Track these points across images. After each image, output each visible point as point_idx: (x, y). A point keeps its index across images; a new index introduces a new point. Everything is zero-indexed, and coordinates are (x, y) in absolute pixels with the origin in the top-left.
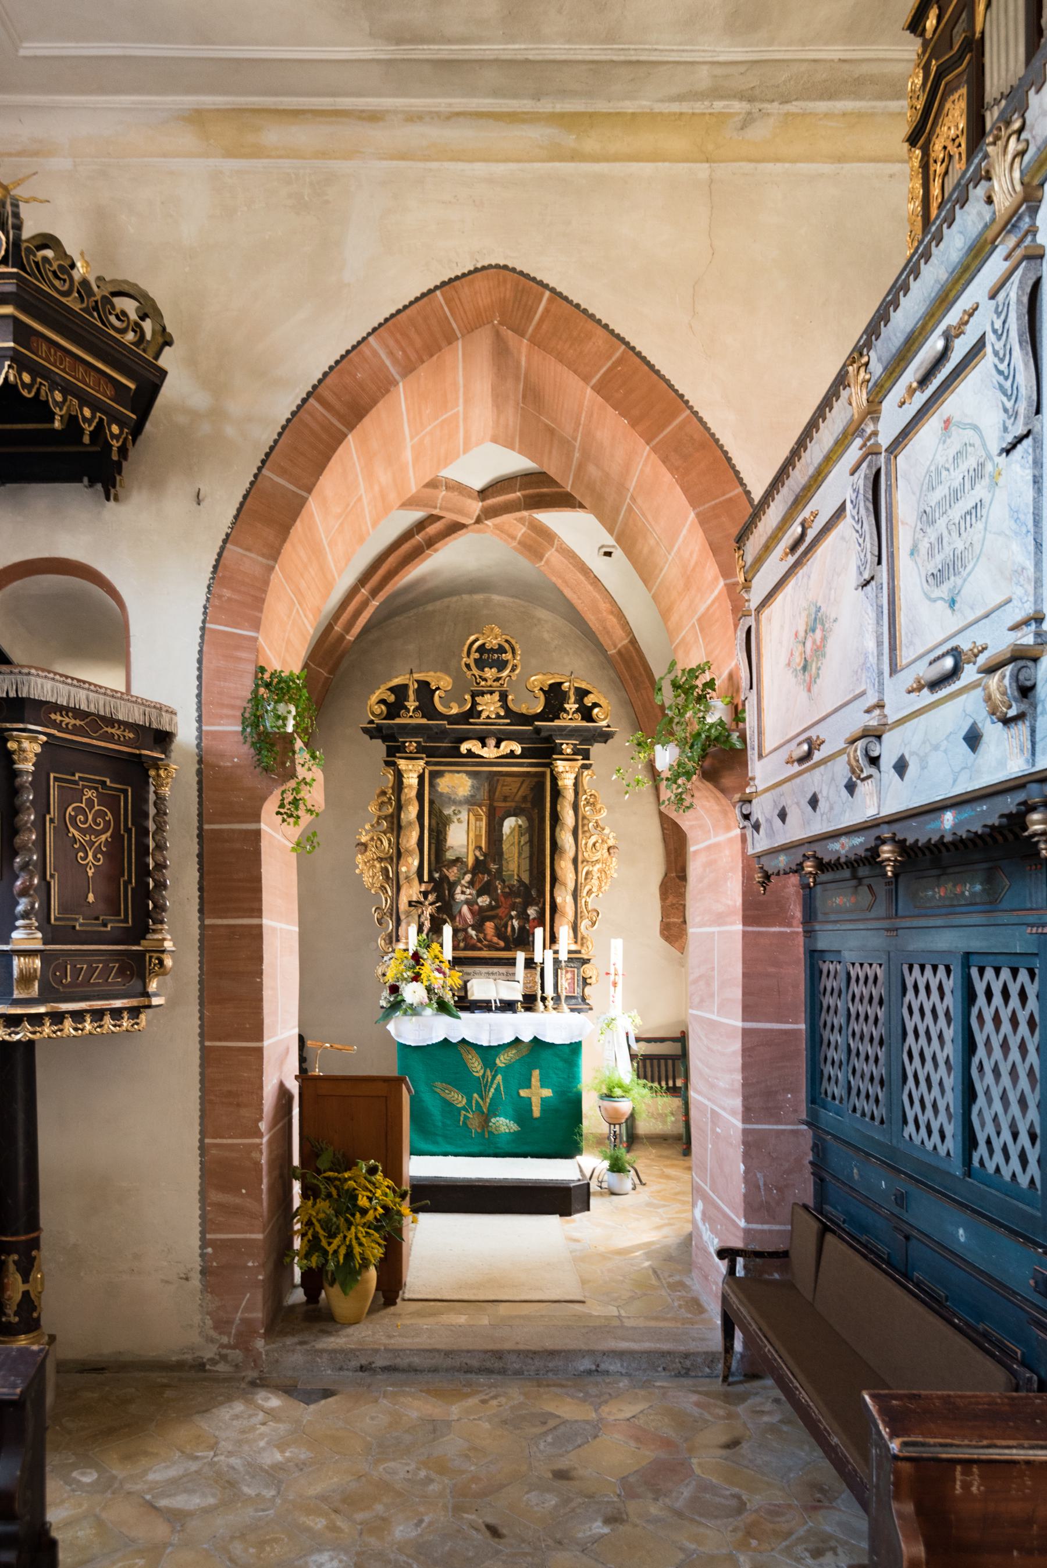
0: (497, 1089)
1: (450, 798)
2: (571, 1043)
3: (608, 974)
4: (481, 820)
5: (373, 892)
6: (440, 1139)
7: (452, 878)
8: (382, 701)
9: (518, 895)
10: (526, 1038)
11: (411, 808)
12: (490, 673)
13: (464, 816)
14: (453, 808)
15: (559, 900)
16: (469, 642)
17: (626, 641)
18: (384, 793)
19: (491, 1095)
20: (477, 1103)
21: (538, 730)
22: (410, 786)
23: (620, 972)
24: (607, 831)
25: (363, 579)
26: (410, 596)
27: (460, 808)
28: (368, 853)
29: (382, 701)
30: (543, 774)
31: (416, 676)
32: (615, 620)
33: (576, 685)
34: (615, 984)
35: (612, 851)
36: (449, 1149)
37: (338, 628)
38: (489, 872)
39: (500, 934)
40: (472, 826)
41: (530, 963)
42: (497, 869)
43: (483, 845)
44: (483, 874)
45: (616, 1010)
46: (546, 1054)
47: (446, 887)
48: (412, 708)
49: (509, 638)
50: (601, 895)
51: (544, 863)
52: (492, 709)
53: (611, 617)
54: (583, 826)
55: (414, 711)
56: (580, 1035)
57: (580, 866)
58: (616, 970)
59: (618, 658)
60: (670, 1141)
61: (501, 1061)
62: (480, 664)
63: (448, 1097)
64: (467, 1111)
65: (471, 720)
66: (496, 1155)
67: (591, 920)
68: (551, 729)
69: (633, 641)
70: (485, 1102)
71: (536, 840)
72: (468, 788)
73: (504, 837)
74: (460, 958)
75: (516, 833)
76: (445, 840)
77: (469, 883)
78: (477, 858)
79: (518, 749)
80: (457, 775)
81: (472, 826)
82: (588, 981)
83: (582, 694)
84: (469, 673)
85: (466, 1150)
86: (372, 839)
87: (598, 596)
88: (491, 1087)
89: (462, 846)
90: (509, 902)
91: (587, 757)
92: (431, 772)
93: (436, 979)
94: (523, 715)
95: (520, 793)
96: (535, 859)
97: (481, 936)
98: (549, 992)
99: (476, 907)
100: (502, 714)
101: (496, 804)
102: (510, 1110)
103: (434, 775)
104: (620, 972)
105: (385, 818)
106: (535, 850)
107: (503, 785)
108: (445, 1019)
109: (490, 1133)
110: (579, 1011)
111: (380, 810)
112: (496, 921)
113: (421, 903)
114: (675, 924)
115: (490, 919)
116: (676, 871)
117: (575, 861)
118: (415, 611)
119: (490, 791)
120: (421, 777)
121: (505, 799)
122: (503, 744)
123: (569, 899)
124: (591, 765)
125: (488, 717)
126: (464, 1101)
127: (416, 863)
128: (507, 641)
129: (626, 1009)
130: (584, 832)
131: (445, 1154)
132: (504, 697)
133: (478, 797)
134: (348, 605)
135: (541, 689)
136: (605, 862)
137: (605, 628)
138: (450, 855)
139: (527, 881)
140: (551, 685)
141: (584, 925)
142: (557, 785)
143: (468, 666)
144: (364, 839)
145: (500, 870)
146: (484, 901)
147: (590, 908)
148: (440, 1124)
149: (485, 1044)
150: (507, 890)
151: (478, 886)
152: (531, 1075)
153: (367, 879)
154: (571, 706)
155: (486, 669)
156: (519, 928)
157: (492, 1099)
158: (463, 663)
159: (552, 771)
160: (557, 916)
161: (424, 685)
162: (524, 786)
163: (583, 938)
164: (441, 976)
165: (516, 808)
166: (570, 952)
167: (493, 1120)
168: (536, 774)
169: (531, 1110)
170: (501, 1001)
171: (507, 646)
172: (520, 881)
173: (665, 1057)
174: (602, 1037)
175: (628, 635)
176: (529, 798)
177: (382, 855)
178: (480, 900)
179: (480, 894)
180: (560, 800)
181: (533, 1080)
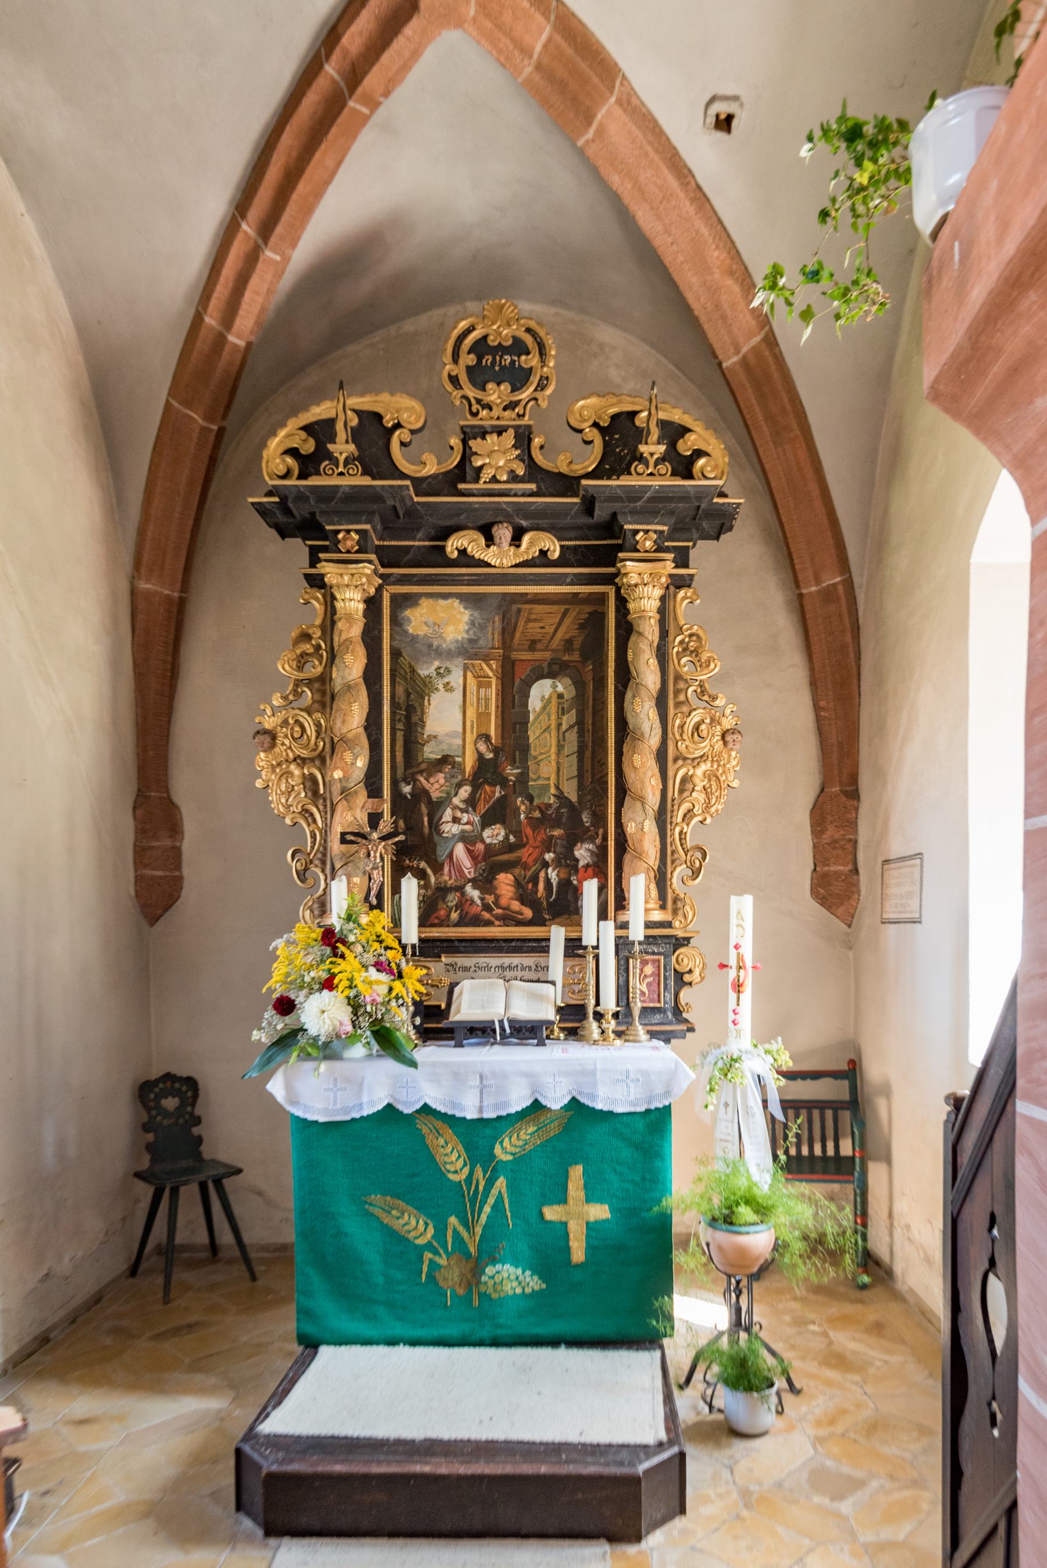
0: (498, 1206)
1: (430, 646)
2: (648, 1111)
3: (723, 966)
4: (489, 685)
5: (288, 821)
6: (381, 1311)
7: (435, 795)
8: (293, 452)
9: (556, 823)
10: (556, 1100)
11: (349, 658)
12: (496, 394)
13: (456, 678)
14: (437, 664)
15: (631, 828)
16: (455, 333)
17: (757, 339)
18: (306, 637)
20: (456, 1233)
21: (589, 504)
22: (349, 618)
23: (749, 961)
24: (720, 702)
25: (241, 207)
26: (363, 288)
27: (448, 664)
29: (293, 452)
30: (602, 598)
31: (353, 402)
33: (662, 415)
34: (738, 987)
35: (729, 738)
36: (399, 1329)
37: (210, 320)
38: (503, 782)
39: (525, 896)
40: (472, 698)
41: (574, 947)
42: (517, 776)
43: (493, 733)
44: (493, 785)
46: (597, 1133)
47: (424, 810)
50: (709, 821)
51: (604, 764)
52: (501, 463)
53: (729, 282)
54: (677, 692)
56: (667, 1093)
57: (671, 769)
58: (740, 958)
61: (505, 1150)
62: (478, 376)
64: (436, 1253)
65: (461, 486)
66: (496, 1343)
67: (691, 867)
69: (771, 341)
72: (463, 627)
74: (654, 937)
75: (553, 708)
77: (465, 801)
78: (480, 756)
79: (554, 548)
81: (472, 698)
82: (687, 978)
83: (674, 432)
84: (457, 394)
86: (285, 722)
88: (484, 1202)
89: (452, 735)
90: (542, 836)
91: (682, 559)
94: (561, 475)
95: (559, 635)
96: (588, 754)
97: (490, 899)
98: (609, 1003)
99: (480, 847)
101: (515, 655)
102: (523, 1248)
103: (401, 602)
104: (749, 961)
105: (309, 683)
106: (589, 738)
107: (529, 620)
108: (390, 1066)
109: (484, 1296)
110: (666, 1037)
111: (300, 668)
112: (517, 871)
113: (363, 836)
114: (837, 874)
115: (506, 867)
116: (841, 785)
117: (661, 756)
118: (381, 334)
119: (504, 631)
120: (372, 604)
121: (533, 645)
122: (526, 539)
123: (650, 826)
124: (691, 576)
125: (494, 479)
126: (431, 1231)
127: (362, 763)
128: (528, 330)
129: (762, 1036)
130: (678, 705)
131: (392, 1342)
133: (482, 643)
135: (595, 425)
136: (716, 759)
137: (718, 307)
138: (430, 752)
139: (574, 798)
140: (615, 417)
141: (678, 874)
142: (627, 612)
144: (269, 722)
145: (523, 778)
146: (495, 834)
147: (689, 844)
148: (380, 1280)
149: (471, 1115)
150: (537, 814)
151: (482, 808)
153: (276, 801)
155: (490, 386)
156: (560, 884)
157: (486, 1227)
158: (445, 374)
159: (618, 589)
160: (627, 858)
161: (371, 419)
162: (568, 621)
164: (383, 977)
165: (552, 663)
166: (648, 925)
167: (489, 1270)
168: (590, 599)
169: (568, 1249)
170: (511, 1022)
171: (529, 340)
172: (560, 796)
173: (821, 1105)
174: (713, 1099)
175: (762, 327)
176: (577, 644)
177: (304, 753)
178: (487, 833)
179: (487, 821)
180: (633, 638)
181: (570, 1186)
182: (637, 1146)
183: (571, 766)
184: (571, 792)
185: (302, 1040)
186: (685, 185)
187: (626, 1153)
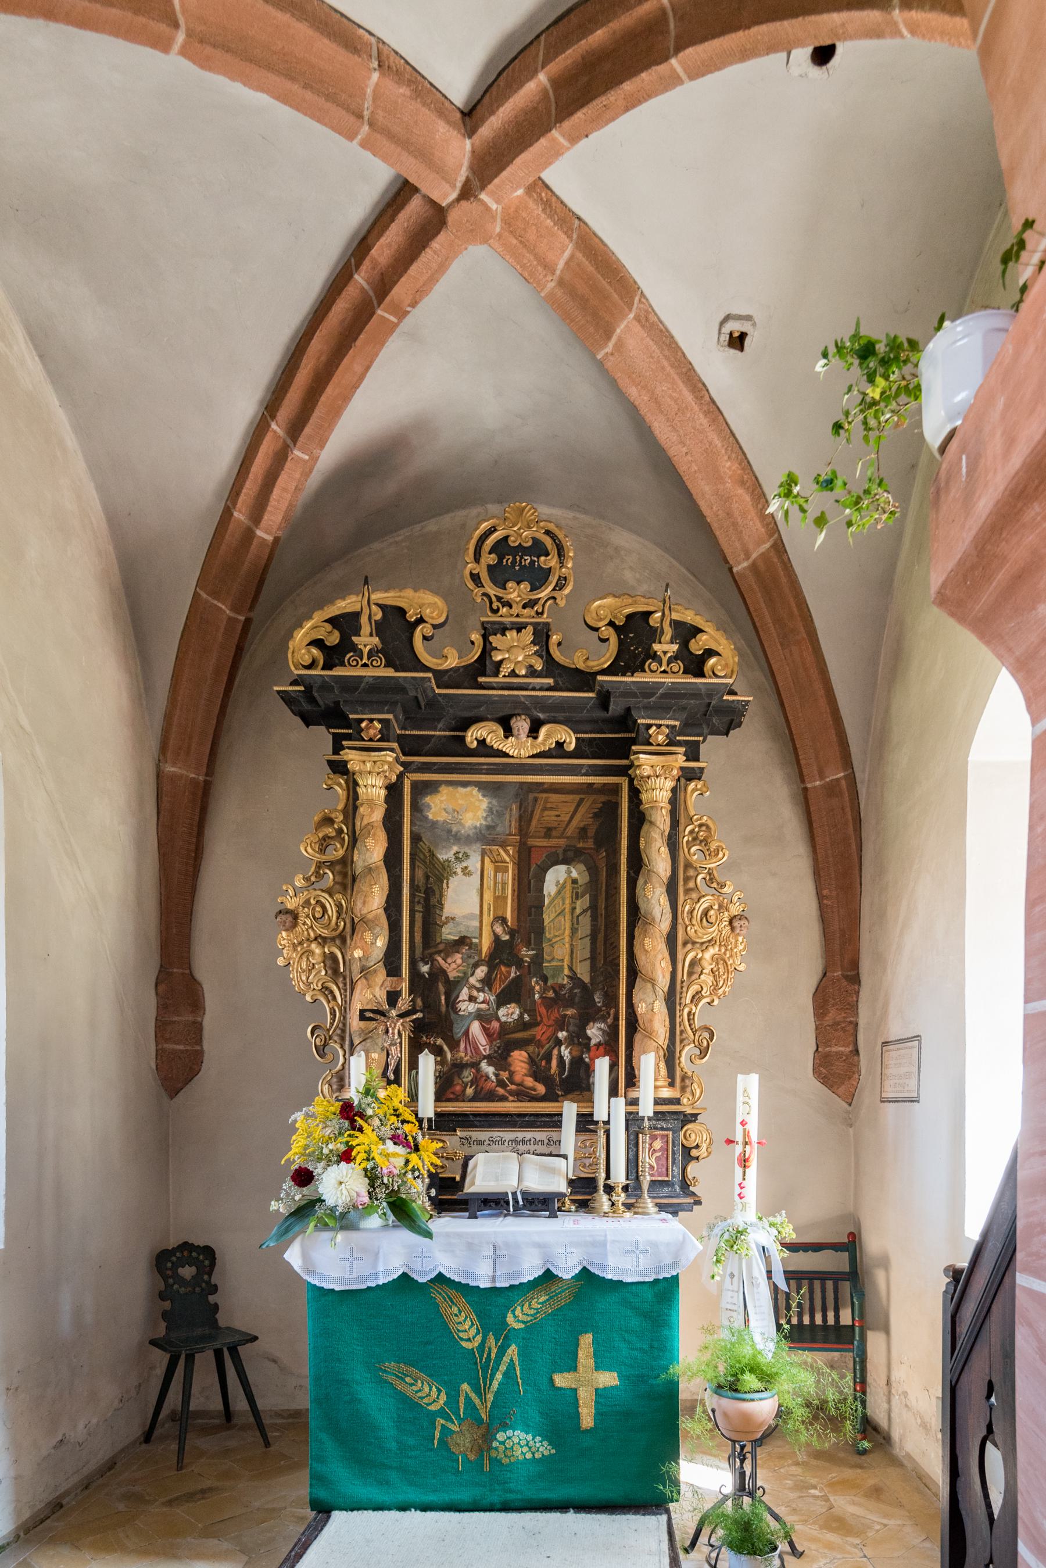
1: (449, 831)
3: (729, 1142)
4: (506, 870)
5: (308, 998)
6: (393, 1476)
7: (452, 975)
8: (318, 643)
9: (570, 1003)
10: (567, 1269)
11: (370, 842)
12: (516, 592)
13: (474, 862)
14: (455, 849)
15: (641, 1009)
16: (478, 533)
17: (768, 545)
19: (495, 1385)
22: (371, 803)
23: (754, 1137)
25: (271, 407)
27: (466, 849)
28: (298, 929)
29: (318, 643)
30: (616, 789)
32: (747, 498)
33: (675, 616)
34: (744, 1162)
35: (736, 924)
37: (239, 515)
38: (519, 963)
39: (538, 1074)
40: (489, 882)
41: (586, 1123)
42: (532, 957)
43: (509, 916)
45: (747, 1214)
46: (607, 1303)
47: (442, 989)
48: (366, 651)
49: (551, 527)
50: (716, 1002)
51: (616, 947)
53: (740, 491)
54: (687, 879)
55: (370, 655)
56: (675, 1264)
59: (752, 580)
60: (530, 687)
61: (516, 1319)
62: (499, 575)
63: (410, 1391)
65: (481, 679)
67: (699, 1046)
68: (627, 692)
69: (779, 548)
70: (484, 1401)
71: (602, 905)
72: (481, 813)
73: (547, 902)
75: (568, 893)
76: (441, 906)
77: (481, 981)
78: (497, 938)
79: (570, 740)
80: (461, 790)
81: (489, 882)
83: (686, 633)
84: (479, 591)
85: (445, 1497)
86: (307, 903)
87: (718, 442)
89: (470, 917)
91: (693, 754)
92: (415, 785)
93: (387, 1156)
95: (574, 823)
96: (601, 937)
97: (504, 1075)
98: (620, 1176)
99: (495, 1025)
100: (539, 666)
101: (532, 842)
102: (534, 1415)
103: (422, 789)
104: (754, 1137)
105: (331, 865)
106: (602, 922)
107: (545, 809)
109: (495, 1462)
110: (674, 1210)
111: (322, 851)
112: (531, 1049)
114: (839, 1054)
115: (520, 1044)
116: (842, 970)
118: (404, 533)
119: (520, 818)
121: (548, 832)
122: (543, 731)
123: (660, 1007)
124: (702, 769)
125: (513, 674)
126: (443, 1398)
127: (381, 943)
128: (548, 533)
129: (767, 1210)
130: (687, 891)
131: (403, 1508)
132: (542, 635)
133: (499, 829)
134: (251, 463)
135: (611, 624)
136: (724, 943)
137: (729, 514)
138: (448, 933)
139: (586, 979)
140: (630, 617)
141: (686, 1054)
143: (476, 578)
145: (538, 960)
146: (509, 1013)
147: (697, 1024)
148: (393, 1445)
151: (498, 988)
152: (577, 1345)
153: (297, 979)
154: (666, 647)
155: (510, 585)
156: (572, 1062)
158: (467, 572)
159: (631, 781)
160: (638, 1037)
162: (582, 810)
163: (684, 1078)
167: (500, 1436)
168: (605, 789)
171: (548, 541)
172: (573, 977)
173: (822, 1276)
174: (719, 1269)
175: (771, 536)
176: (591, 832)
178: (502, 1012)
179: (503, 1000)
180: (645, 827)
182: (645, 1315)
183: (584, 949)
184: (585, 976)
185: (320, 1211)
186: (699, 398)
187: (635, 1322)
